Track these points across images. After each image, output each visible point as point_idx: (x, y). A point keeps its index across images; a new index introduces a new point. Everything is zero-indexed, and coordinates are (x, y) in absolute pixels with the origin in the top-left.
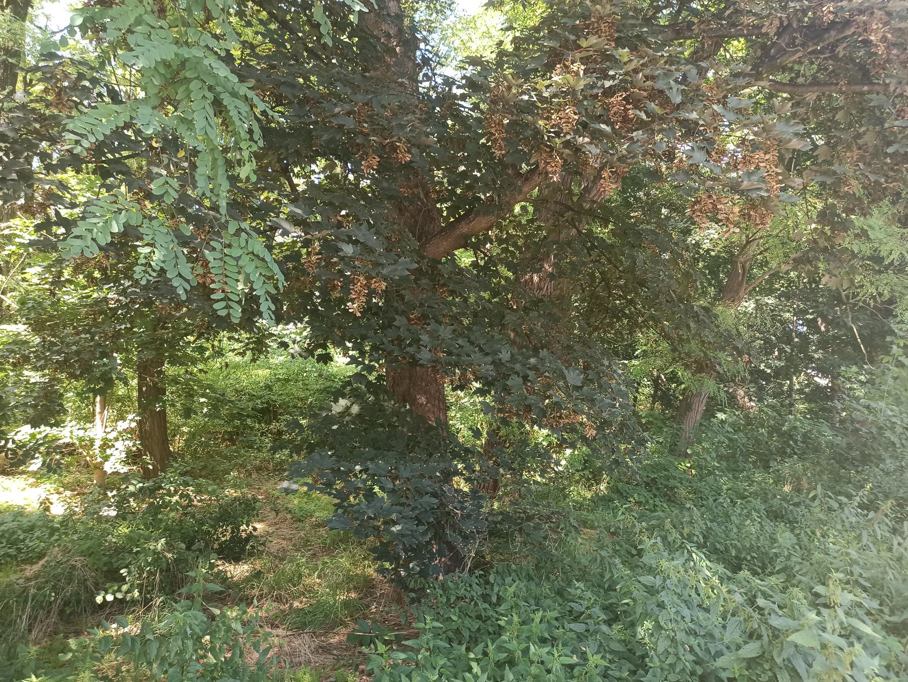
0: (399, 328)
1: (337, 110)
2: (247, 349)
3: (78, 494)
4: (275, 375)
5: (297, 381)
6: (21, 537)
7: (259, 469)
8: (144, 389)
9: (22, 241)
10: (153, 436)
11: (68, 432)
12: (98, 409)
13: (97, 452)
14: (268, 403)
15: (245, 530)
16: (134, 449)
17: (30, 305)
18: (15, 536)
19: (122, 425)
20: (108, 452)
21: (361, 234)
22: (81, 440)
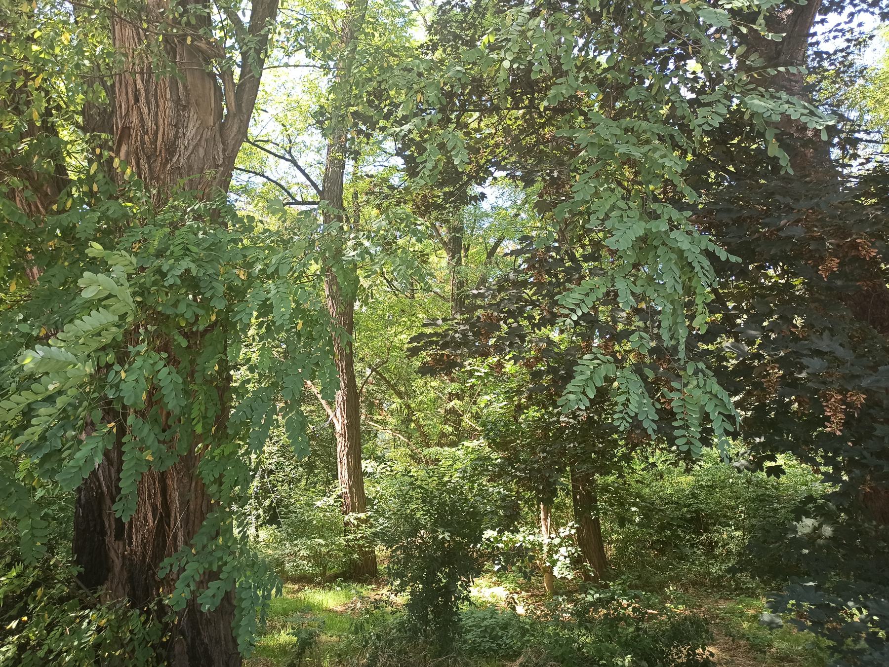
0: (883, 438)
1: (782, 223)
2: (679, 460)
3: (532, 596)
4: (698, 481)
5: (722, 488)
6: (499, 634)
7: (694, 584)
8: (578, 497)
9: (479, 374)
10: (589, 541)
11: (522, 537)
12: (542, 516)
13: (545, 556)
14: (695, 512)
15: (702, 655)
16: (576, 555)
17: (489, 427)
18: (495, 633)
19: (564, 532)
20: (555, 557)
21: (824, 345)
22: (532, 543)
